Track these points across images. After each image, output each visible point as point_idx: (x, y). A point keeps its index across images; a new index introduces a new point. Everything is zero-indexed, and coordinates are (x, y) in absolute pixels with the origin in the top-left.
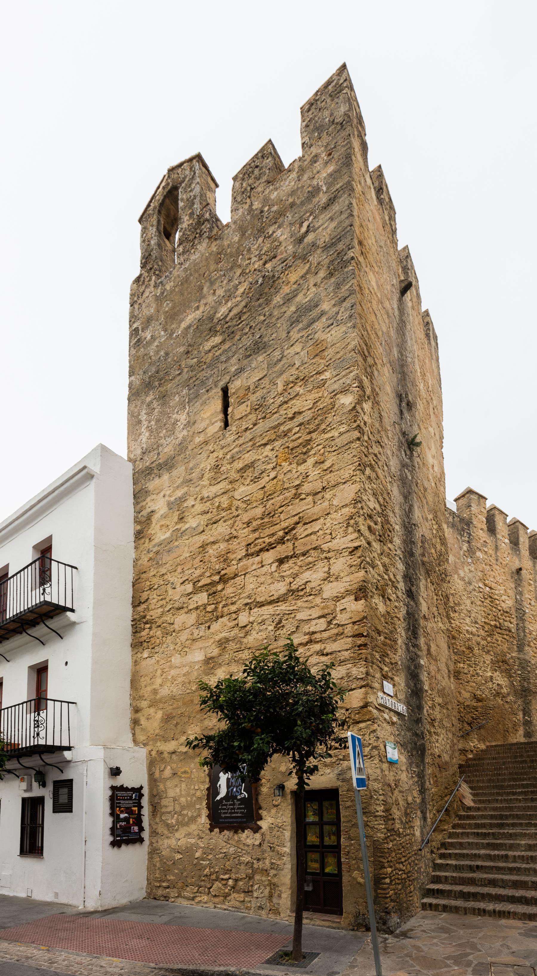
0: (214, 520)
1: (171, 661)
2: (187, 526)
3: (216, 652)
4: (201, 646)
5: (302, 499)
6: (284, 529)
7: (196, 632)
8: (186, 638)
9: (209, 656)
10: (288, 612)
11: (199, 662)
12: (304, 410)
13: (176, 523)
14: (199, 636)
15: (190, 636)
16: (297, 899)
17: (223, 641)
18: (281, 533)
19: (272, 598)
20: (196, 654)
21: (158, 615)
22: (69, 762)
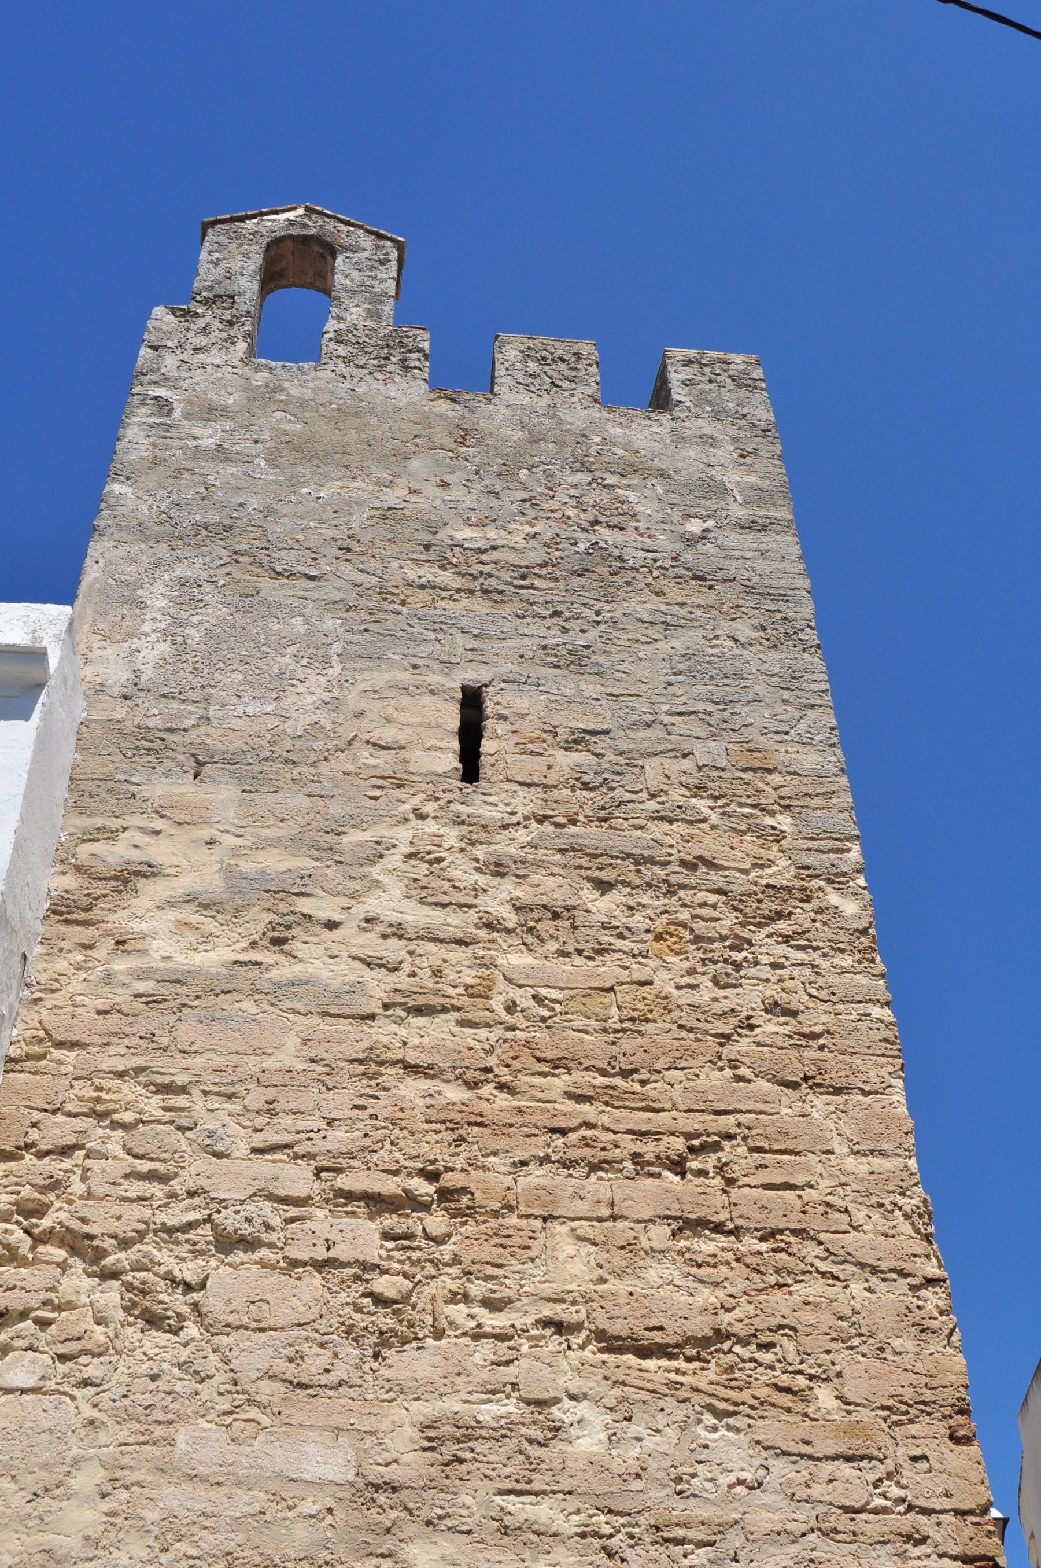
0: (421, 1001)
1: (172, 1443)
2: (297, 970)
3: (412, 1465)
4: (337, 1420)
5: (739, 1079)
6: (688, 1136)
7: (316, 1360)
8: (264, 1366)
9: (375, 1473)
10: (722, 1406)
11: (321, 1484)
12: (726, 864)
13: (253, 945)
14: (332, 1378)
15: (281, 1366)
16: (8, 876)
17: (448, 1430)
18: (679, 1144)
19: (658, 1337)
20: (311, 1448)
21: (126, 1229)
22: (327, 291)
